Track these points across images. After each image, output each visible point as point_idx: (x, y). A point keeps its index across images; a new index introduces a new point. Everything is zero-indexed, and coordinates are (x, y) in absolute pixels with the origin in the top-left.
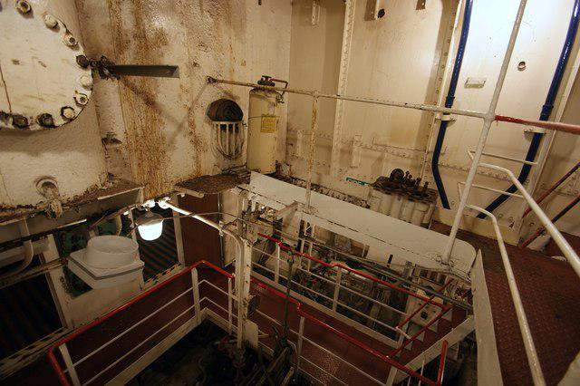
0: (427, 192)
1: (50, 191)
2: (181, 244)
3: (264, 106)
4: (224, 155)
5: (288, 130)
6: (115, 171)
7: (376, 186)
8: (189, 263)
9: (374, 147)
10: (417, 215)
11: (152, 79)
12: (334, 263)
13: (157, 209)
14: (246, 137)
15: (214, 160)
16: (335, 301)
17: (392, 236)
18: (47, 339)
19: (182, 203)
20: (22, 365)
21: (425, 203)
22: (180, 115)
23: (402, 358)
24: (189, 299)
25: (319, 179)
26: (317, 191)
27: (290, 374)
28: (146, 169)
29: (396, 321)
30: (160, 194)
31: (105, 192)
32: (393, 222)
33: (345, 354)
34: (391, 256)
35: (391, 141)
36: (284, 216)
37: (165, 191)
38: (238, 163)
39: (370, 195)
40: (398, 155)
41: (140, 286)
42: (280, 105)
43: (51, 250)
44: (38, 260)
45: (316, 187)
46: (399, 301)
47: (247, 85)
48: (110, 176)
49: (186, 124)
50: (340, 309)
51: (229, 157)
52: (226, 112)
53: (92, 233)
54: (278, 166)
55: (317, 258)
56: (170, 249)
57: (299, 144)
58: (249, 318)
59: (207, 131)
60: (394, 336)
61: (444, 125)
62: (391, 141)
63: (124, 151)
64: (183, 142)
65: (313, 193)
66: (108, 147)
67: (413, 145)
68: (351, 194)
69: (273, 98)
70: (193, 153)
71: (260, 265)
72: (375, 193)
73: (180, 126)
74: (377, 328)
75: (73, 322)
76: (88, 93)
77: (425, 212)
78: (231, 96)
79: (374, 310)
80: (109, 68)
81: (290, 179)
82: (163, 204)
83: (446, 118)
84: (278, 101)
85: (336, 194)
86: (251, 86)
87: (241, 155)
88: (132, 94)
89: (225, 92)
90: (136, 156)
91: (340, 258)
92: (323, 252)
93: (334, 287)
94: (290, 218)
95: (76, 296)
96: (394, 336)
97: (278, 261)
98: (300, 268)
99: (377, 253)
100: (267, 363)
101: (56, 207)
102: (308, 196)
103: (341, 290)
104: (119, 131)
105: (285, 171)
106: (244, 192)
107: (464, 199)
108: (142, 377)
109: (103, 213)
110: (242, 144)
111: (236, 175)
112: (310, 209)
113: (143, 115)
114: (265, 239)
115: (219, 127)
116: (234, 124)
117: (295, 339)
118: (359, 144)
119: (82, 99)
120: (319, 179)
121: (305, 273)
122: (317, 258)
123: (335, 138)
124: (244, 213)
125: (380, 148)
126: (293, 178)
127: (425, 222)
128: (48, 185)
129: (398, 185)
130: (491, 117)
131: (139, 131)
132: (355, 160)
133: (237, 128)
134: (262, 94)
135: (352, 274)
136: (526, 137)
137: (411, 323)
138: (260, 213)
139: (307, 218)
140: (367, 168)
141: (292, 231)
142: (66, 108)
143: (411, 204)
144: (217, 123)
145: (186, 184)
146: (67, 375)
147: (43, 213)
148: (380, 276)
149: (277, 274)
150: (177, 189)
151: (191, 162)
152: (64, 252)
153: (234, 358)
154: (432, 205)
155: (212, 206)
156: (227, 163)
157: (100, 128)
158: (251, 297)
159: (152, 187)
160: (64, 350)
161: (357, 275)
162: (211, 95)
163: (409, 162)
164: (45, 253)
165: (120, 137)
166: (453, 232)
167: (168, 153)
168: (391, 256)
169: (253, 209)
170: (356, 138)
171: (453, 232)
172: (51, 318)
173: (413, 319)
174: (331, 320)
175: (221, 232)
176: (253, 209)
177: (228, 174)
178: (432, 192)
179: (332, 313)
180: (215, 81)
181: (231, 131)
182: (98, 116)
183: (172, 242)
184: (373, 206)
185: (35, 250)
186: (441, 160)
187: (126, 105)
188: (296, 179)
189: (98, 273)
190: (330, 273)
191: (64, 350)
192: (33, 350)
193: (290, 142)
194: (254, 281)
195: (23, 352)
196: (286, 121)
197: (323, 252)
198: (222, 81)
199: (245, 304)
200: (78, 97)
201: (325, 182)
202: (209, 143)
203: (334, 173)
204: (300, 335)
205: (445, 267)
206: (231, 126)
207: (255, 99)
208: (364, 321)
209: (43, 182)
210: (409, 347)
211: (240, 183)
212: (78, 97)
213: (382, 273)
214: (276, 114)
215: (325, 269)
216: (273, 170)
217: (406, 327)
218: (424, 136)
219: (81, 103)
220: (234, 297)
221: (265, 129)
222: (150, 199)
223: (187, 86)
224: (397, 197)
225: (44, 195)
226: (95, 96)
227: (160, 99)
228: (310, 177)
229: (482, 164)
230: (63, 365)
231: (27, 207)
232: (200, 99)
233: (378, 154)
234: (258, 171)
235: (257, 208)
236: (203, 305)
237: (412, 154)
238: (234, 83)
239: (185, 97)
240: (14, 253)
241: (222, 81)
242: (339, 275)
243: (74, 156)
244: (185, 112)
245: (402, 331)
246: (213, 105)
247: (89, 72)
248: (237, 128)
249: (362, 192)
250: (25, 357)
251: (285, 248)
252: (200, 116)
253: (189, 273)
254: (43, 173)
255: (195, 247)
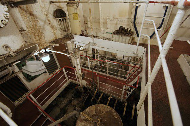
0: (131, 33)
1: (8, 49)
2: (58, 62)
3: (73, 10)
4: (63, 30)
5: (84, 18)
6: (28, 41)
7: (114, 33)
8: (62, 67)
9: (114, 20)
10: (127, 41)
11: (30, 5)
12: (106, 61)
13: (46, 52)
14: (69, 23)
15: (60, 33)
16: (108, 71)
17: (122, 49)
18: (26, 95)
19: (54, 49)
20: (21, 102)
21: (129, 36)
22: (44, 17)
23: (127, 83)
24: (64, 77)
25: (97, 34)
26: (96, 38)
27: (96, 91)
28: (38, 39)
29: (126, 74)
30: (45, 47)
31: (26, 47)
32: (120, 44)
33: (112, 84)
34: (124, 55)
35: (120, 17)
36: (87, 47)
37: (47, 45)
38: (69, 32)
39: (112, 37)
40: (122, 21)
41: (48, 76)
42: (78, 8)
43: (17, 70)
44: (13, 72)
45: (96, 37)
46: (127, 69)
47: (64, 2)
48: (26, 42)
49: (47, 21)
50: (109, 73)
51: (65, 31)
52: (60, 14)
53: (27, 61)
54: (82, 32)
55: (101, 60)
56: (54, 62)
57: (89, 23)
58: (82, 79)
59: (55, 22)
60: (125, 78)
61: (137, 7)
62: (120, 17)
63: (28, 33)
64: (48, 28)
65: (95, 39)
66: (22, 32)
67: (127, 17)
68: (107, 38)
69: (75, 6)
70: (52, 31)
71: (84, 65)
72: (114, 35)
73: (45, 22)
74: (121, 76)
75: (31, 89)
76: (8, 14)
77: (130, 39)
78: (61, 8)
79: (119, 72)
80: (13, 4)
81: (87, 36)
82: (48, 50)
83: (137, 5)
84: (77, 6)
85: (103, 38)
86: (66, 2)
87: (69, 30)
88: (25, 13)
89: (58, 6)
90: (33, 35)
91: (108, 59)
92: (103, 58)
93: (107, 68)
94: (88, 48)
95: (30, 82)
96: (125, 78)
97: (89, 63)
98: (96, 64)
99: (119, 55)
100: (90, 90)
101: (12, 54)
102: (93, 40)
103: (109, 68)
104: (24, 27)
105: (85, 33)
106: (72, 42)
107: (143, 34)
108: (57, 99)
109: (25, 55)
110: (69, 26)
111: (69, 37)
112: (94, 44)
113: (31, 20)
114: (84, 57)
115: (59, 20)
116: (64, 18)
117: (97, 83)
118: (109, 19)
119: (7, 16)
120: (97, 34)
121: (98, 65)
122: (101, 60)
123: (101, 18)
124: (74, 49)
125: (116, 20)
126: (88, 35)
127: (130, 42)
128: (6, 47)
129: (122, 32)
130: (148, 2)
131: (31, 26)
132: (109, 26)
133: (65, 20)
134: (71, 5)
135: (112, 63)
136: (164, 9)
137: (130, 74)
138: (79, 48)
139: (94, 47)
140: (113, 28)
141: (90, 53)
142: (2, 20)
143: (125, 37)
144: (58, 19)
145: (53, 42)
146: (34, 102)
147: (8, 56)
148: (121, 62)
149: (89, 67)
150: (50, 44)
151: (53, 34)
152: (21, 69)
153: (80, 90)
154: (132, 37)
155: (63, 48)
156: (65, 33)
157: (17, 27)
158: (82, 74)
159: (42, 45)
160: (31, 96)
161: (113, 63)
162: (53, 8)
163: (126, 23)
164: (15, 70)
165: (25, 29)
166: (138, 44)
167: (44, 32)
168: (124, 55)
169: (77, 47)
170: (108, 18)
171: (138, 44)
172: (25, 90)
173: (130, 72)
174: (107, 77)
175: (68, 56)
176: (77, 47)
177: (66, 37)
178: (133, 33)
179: (107, 75)
180: (53, 2)
181: (63, 21)
182: (15, 22)
183: (54, 60)
184: (114, 40)
185: (12, 69)
186: (136, 21)
187: (24, 17)
188: (89, 35)
189: (32, 72)
190: (105, 64)
191: (31, 96)
192: (23, 98)
193: (86, 23)
194: (82, 70)
195: (20, 99)
196: (83, 14)
197: (103, 58)
198: (56, 2)
199: (80, 76)
200: (5, 16)
201: (99, 34)
202: (57, 26)
203: (102, 31)
204: (98, 81)
205: (136, 55)
206: (63, 19)
207: (69, 7)
208: (117, 76)
209: (5, 46)
210: (129, 80)
211: (70, 39)
212: (5, 16)
213: (121, 62)
214: (78, 12)
215: (104, 63)
216: (81, 33)
217: (128, 75)
218: (130, 13)
219: (7, 17)
220: (78, 75)
221: (75, 18)
222: (42, 49)
223: (43, 6)
224: (121, 36)
225: (7, 51)
226: (12, 15)
227: (35, 13)
228: (92, 33)
229: (146, 20)
230: (33, 100)
231: (3, 55)
232: (49, 10)
233: (115, 22)
234: (75, 34)
235: (78, 47)
236: (69, 78)
237: (126, 20)
238: (60, 2)
239: (44, 10)
240: (5, 71)
241: (56, 2)
242: (108, 64)
243: (12, 37)
244: (45, 16)
245: (128, 76)
246: (55, 12)
247: (6, 6)
248: (65, 20)
249: (110, 36)
250: (21, 100)
251: (90, 58)
252: (51, 17)
253: (63, 71)
254: (4, 44)
255: (60, 63)
